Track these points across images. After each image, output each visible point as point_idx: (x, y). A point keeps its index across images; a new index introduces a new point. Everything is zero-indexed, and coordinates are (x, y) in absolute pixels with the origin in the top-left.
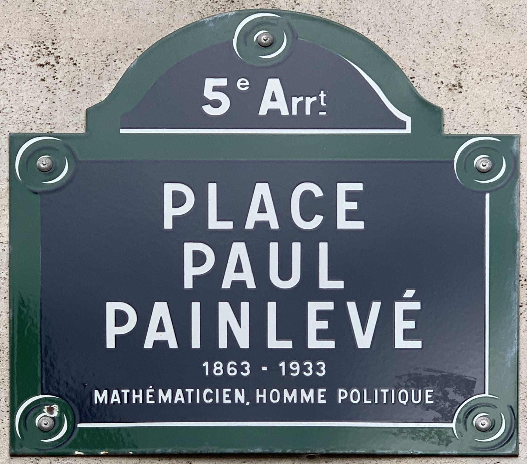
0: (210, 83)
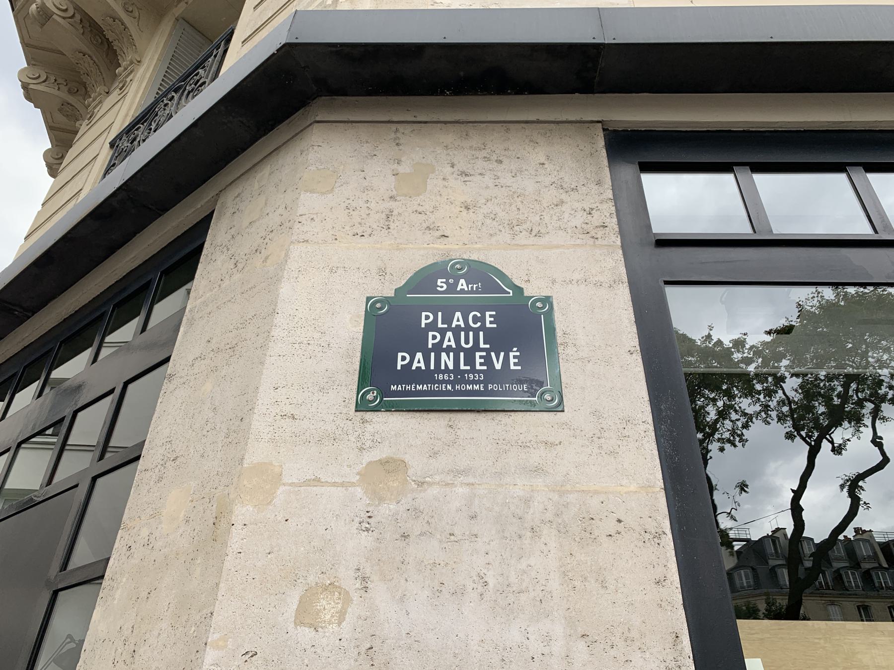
0: (439, 281)
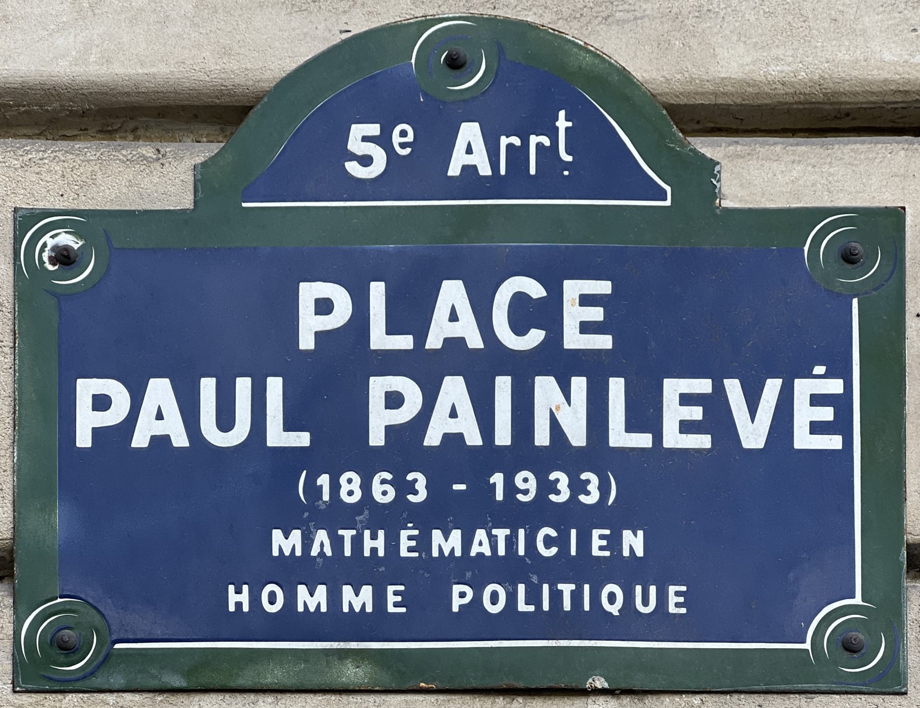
0: (358, 131)
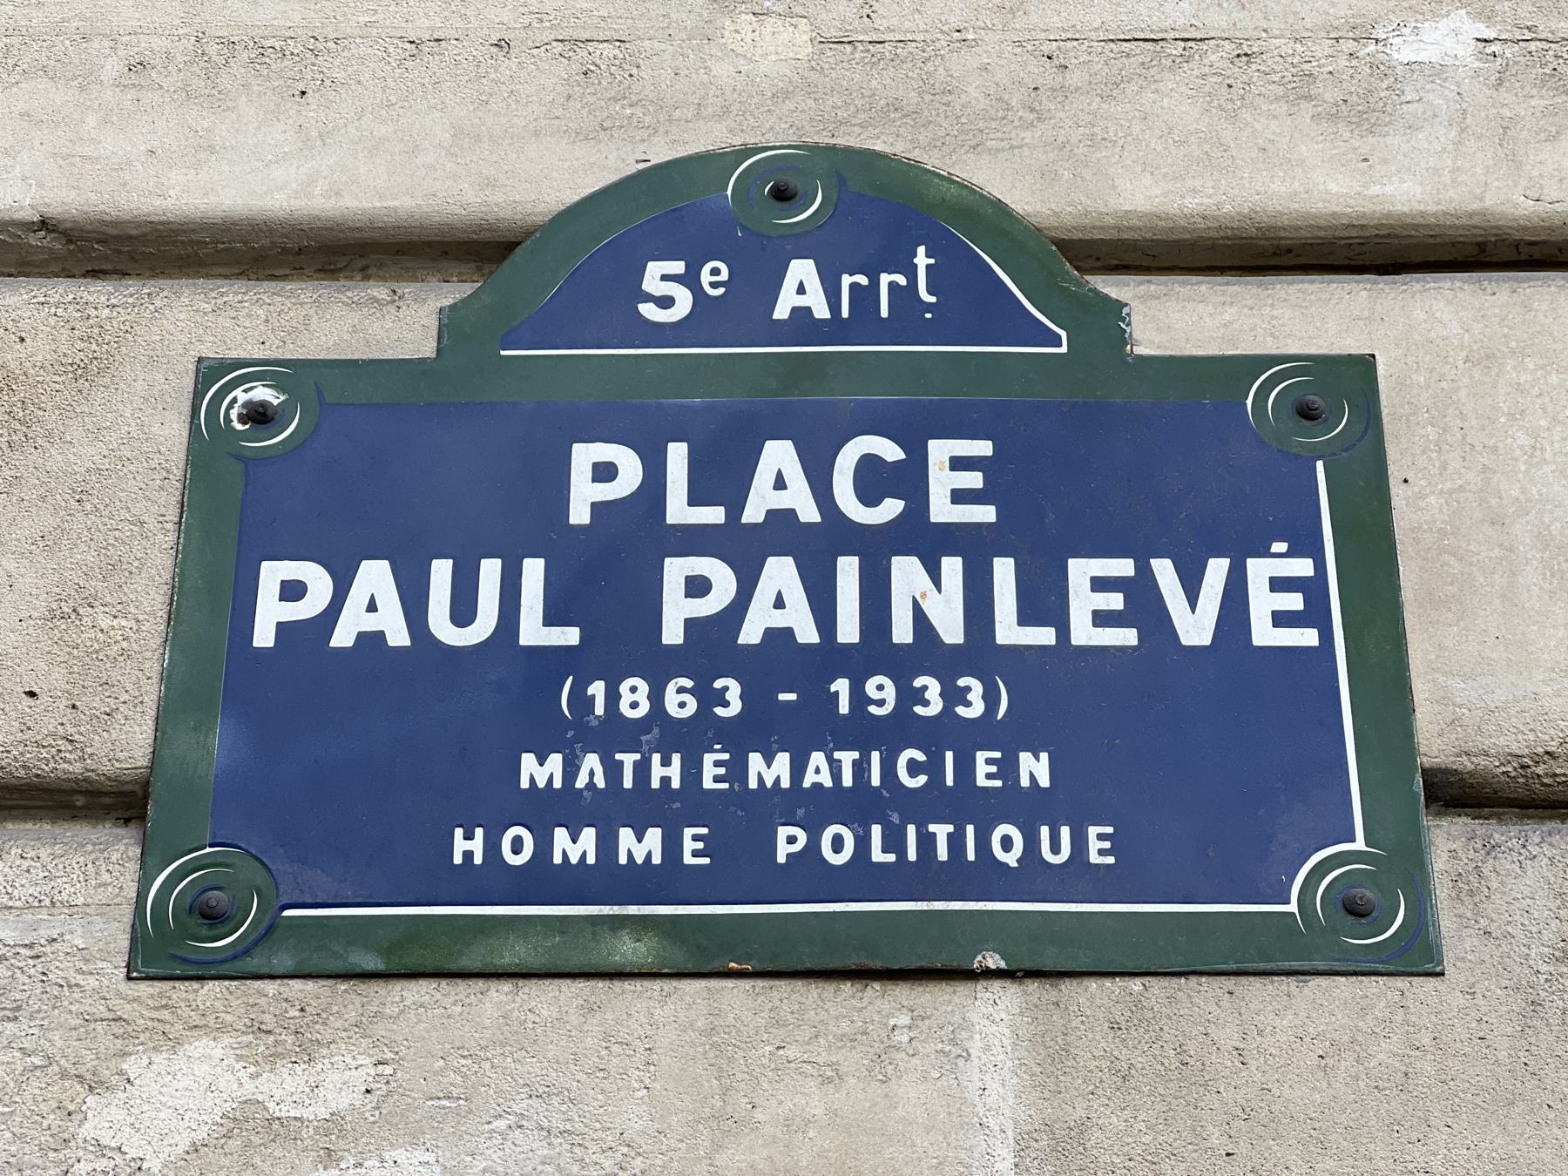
0: (655, 269)
